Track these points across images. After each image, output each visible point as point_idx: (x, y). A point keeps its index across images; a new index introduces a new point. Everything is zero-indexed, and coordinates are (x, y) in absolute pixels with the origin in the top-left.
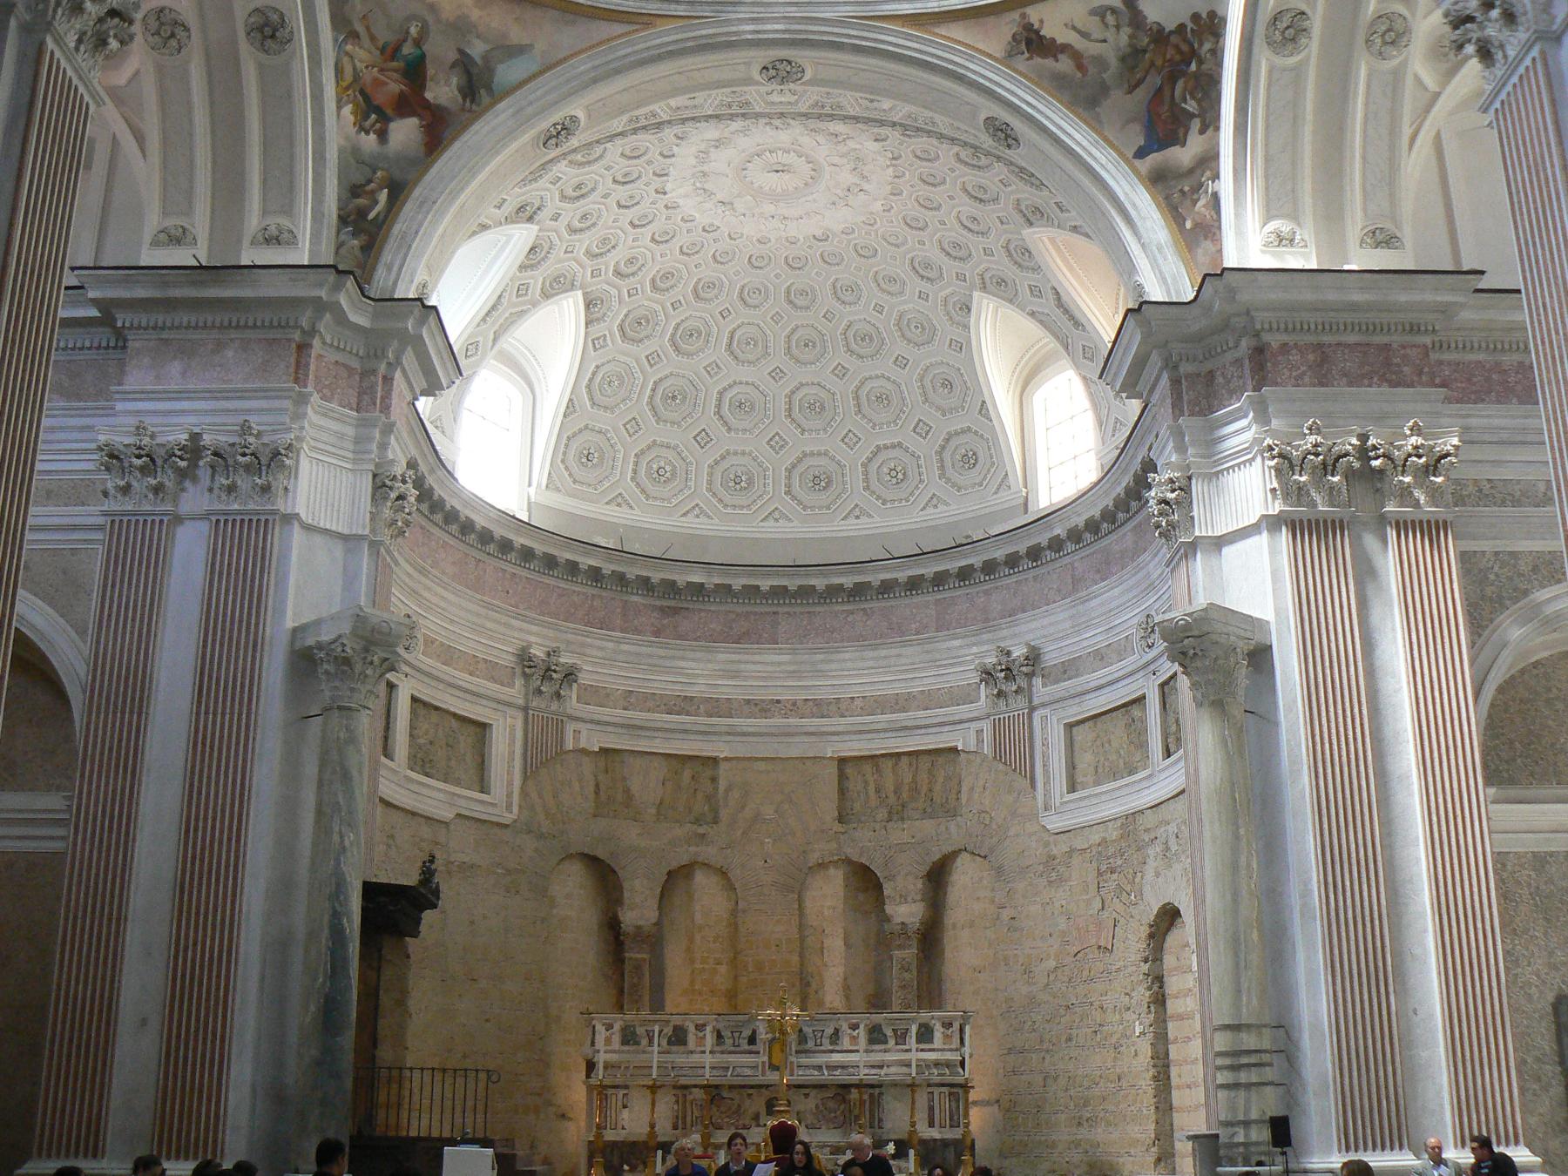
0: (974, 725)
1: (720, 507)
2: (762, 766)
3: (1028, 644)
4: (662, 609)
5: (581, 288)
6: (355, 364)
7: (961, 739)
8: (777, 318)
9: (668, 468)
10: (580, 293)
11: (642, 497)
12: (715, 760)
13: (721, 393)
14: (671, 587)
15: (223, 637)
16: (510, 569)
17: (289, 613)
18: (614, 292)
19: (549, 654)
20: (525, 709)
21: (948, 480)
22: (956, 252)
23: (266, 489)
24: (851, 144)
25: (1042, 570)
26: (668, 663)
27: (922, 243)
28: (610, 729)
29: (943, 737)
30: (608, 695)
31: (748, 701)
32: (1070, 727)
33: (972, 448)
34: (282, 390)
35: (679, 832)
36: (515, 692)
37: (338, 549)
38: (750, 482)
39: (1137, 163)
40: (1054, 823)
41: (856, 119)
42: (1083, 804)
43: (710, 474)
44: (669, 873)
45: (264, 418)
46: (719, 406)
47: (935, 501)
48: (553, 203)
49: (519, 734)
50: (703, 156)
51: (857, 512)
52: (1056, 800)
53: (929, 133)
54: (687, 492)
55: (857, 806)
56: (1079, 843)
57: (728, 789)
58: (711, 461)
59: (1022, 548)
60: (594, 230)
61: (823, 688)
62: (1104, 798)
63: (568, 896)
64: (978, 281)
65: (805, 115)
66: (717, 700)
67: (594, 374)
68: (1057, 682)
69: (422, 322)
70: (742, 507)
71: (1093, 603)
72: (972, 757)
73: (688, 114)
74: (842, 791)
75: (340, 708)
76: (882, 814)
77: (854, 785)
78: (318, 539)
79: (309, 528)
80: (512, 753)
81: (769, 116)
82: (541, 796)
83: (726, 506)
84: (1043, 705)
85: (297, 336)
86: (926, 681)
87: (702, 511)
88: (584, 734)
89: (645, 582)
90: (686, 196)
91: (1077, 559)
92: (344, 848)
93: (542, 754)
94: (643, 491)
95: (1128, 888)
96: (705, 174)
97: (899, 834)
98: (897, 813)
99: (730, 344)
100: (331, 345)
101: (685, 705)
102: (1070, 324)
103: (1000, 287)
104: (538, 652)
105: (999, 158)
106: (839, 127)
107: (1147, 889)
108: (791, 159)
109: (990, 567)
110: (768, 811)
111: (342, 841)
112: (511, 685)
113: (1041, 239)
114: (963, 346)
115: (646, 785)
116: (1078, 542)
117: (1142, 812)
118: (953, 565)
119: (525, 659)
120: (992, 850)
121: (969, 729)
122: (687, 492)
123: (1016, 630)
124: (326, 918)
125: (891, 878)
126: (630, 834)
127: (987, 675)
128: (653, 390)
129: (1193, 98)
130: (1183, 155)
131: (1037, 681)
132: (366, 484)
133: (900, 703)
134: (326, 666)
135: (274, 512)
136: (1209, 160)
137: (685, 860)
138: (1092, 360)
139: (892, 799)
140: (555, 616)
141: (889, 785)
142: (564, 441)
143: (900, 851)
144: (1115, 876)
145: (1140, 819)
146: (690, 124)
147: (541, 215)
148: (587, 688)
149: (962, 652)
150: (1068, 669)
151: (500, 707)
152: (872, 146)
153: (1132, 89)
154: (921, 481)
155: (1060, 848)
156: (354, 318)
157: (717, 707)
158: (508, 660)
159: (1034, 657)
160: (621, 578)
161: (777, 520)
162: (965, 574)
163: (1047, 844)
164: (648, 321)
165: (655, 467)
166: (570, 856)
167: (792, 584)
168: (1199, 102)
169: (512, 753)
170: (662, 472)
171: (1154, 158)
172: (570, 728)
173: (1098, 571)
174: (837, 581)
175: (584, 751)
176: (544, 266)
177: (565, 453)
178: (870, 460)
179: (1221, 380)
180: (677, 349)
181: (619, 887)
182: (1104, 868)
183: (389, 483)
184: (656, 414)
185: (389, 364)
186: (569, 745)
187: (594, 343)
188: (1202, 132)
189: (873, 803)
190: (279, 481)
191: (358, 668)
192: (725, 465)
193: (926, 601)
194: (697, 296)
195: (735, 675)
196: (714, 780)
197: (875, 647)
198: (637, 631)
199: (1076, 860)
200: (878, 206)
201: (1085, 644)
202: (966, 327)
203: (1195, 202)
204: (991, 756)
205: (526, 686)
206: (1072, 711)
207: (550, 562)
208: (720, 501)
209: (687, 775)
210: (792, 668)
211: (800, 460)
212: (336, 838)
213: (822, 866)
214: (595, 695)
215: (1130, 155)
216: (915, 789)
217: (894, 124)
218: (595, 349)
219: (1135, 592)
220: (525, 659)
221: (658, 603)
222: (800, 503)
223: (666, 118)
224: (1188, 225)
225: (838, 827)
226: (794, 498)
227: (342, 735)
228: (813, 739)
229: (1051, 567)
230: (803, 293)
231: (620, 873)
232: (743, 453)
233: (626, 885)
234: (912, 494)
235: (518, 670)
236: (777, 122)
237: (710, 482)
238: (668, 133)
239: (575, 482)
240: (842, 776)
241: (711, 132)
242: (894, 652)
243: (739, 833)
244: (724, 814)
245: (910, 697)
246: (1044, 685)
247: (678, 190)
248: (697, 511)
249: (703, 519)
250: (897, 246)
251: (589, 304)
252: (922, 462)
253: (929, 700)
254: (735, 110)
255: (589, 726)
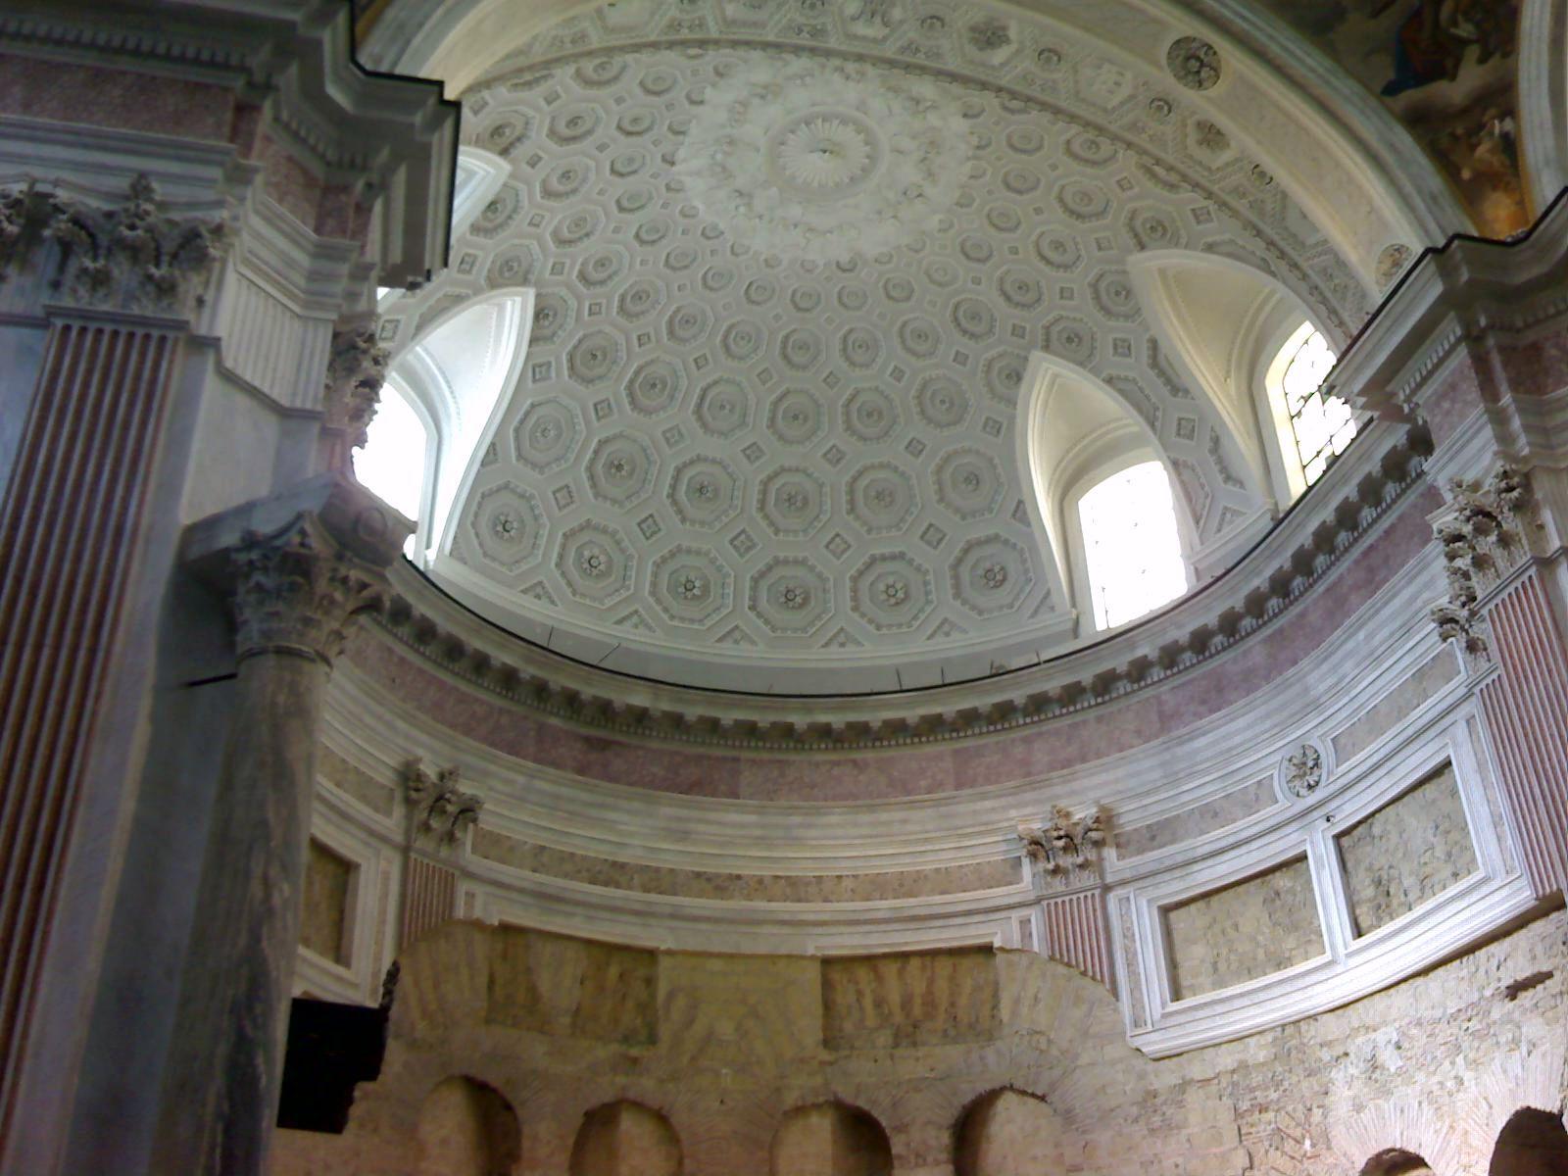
0: (1016, 915)
1: (665, 617)
2: (716, 965)
3: (1097, 802)
4: (587, 740)
5: (537, 285)
6: (318, 170)
7: (1000, 933)
8: (764, 376)
9: (602, 558)
10: (531, 293)
11: (569, 591)
12: (651, 955)
13: (679, 471)
14: (605, 710)
15: (54, 513)
16: (401, 650)
17: (185, 500)
18: (573, 303)
19: (442, 777)
20: (405, 850)
21: (965, 602)
22: (1020, 294)
23: (166, 290)
24: (933, 119)
25: (1113, 707)
26: (594, 812)
27: (977, 281)
28: (514, 895)
29: (973, 931)
30: (512, 849)
31: (698, 875)
32: (1166, 911)
33: (1005, 557)
34: (211, 150)
35: (603, 1052)
36: (392, 823)
37: (270, 424)
38: (706, 589)
39: (1388, 100)
40: (1154, 1043)
41: (954, 77)
42: (1200, 1014)
43: (655, 575)
44: (587, 1114)
45: (180, 188)
46: (674, 487)
47: (946, 628)
48: (538, 140)
49: (394, 888)
50: (739, 111)
51: (842, 638)
52: (1341, 951)
53: (1044, 106)
54: (624, 594)
55: (848, 1027)
56: (1197, 1070)
57: (671, 995)
58: (656, 557)
59: (1086, 676)
60: (573, 199)
61: (800, 861)
62: (1238, 1003)
63: (445, 1142)
64: (1040, 337)
65: (892, 63)
66: (657, 870)
67: (527, 414)
68: (1141, 851)
69: (435, 124)
70: (692, 621)
71: (1201, 742)
72: (1015, 957)
73: (744, 34)
74: (828, 1006)
75: (281, 651)
76: (884, 1038)
77: (844, 997)
78: (242, 401)
79: (229, 377)
80: (383, 912)
81: (845, 56)
82: (416, 983)
83: (672, 617)
84: (1124, 883)
85: (239, 83)
86: (944, 856)
87: (642, 621)
88: (479, 902)
89: (572, 699)
90: (698, 173)
91: (1164, 690)
92: (270, 911)
93: (424, 918)
94: (569, 584)
95: (1298, 1133)
96: (732, 142)
97: (912, 1065)
98: (907, 1035)
99: (700, 405)
100: (287, 126)
101: (613, 873)
102: (1165, 391)
103: (1073, 344)
104: (430, 770)
105: (1129, 145)
106: (926, 88)
107: (1338, 1134)
108: (846, 134)
109: (1039, 704)
110: (726, 1029)
111: (268, 896)
112: (388, 813)
113: (1148, 265)
114: (1004, 430)
115: (560, 983)
116: (1138, 681)
117: (1314, 1017)
118: (984, 701)
119: (409, 777)
120: (1053, 1086)
121: (1014, 921)
122: (624, 594)
123: (1076, 785)
124: (223, 1049)
125: (901, 1128)
126: (536, 1052)
127: (1037, 847)
128: (596, 452)
129: (1468, 20)
130: (1456, 90)
131: (1110, 853)
132: (321, 343)
133: (908, 884)
134: (258, 577)
135: (181, 326)
136: (1501, 97)
137: (607, 1098)
138: (1190, 437)
139: (898, 1018)
140: (453, 726)
141: (894, 997)
142: (478, 498)
143: (915, 1097)
144: (1270, 1115)
145: (1309, 1030)
146: (741, 52)
147: (520, 151)
148: (496, 840)
149: (994, 817)
150: (1156, 835)
151: (372, 841)
152: (958, 124)
153: (1376, 14)
154: (928, 602)
155: (1165, 1078)
156: (334, 92)
157: (657, 880)
158: (386, 777)
159: (1105, 820)
160: (541, 690)
161: (736, 642)
162: (1004, 713)
163: (1142, 1076)
164: (605, 356)
165: (587, 554)
166: (449, 1080)
167: (764, 719)
168: (1477, 24)
169: (383, 912)
170: (594, 562)
171: (1411, 96)
172: (463, 887)
173: (1203, 702)
174: (823, 718)
175: (478, 925)
176: (502, 235)
177: (476, 515)
178: (861, 573)
179: (1554, 352)
180: (633, 402)
181: (513, 1133)
182: (1244, 1106)
183: (363, 345)
184: (594, 486)
185: (369, 186)
186: (460, 912)
187: (533, 371)
188: (1483, 60)
189: (871, 1021)
190: (192, 284)
191: (322, 586)
192: (671, 566)
193: (940, 749)
194: (671, 333)
195: (684, 836)
196: (650, 982)
197: (872, 809)
198: (556, 764)
199: (1193, 1097)
200: (934, 222)
201: (1186, 798)
202: (1012, 402)
203: (1473, 148)
204: (1045, 954)
205: (409, 817)
206: (1165, 889)
207: (454, 650)
208: (666, 610)
209: (613, 971)
210: (758, 832)
211: (770, 568)
212: (256, 889)
213: (800, 1110)
214: (496, 846)
215: (1378, 90)
216: (930, 1002)
217: (999, 90)
218: (535, 380)
219: (1276, 719)
220: (409, 777)
221: (585, 731)
222: (767, 622)
223: (714, 34)
224: (1466, 174)
225: (825, 1055)
226: (759, 615)
227: (281, 699)
228: (786, 930)
229: (1123, 703)
230: (803, 346)
231: (521, 1113)
232: (698, 553)
233: (526, 1130)
234: (915, 618)
235: (399, 795)
236: (851, 67)
237: (654, 585)
238: (712, 57)
239: (485, 555)
240: (827, 985)
241: (760, 70)
242: (898, 815)
243: (685, 1060)
244: (665, 1032)
245: (920, 878)
246: (1120, 857)
247: (692, 161)
248: (635, 619)
249: (641, 630)
250: (940, 285)
251: (540, 315)
252: (930, 577)
253: (946, 880)
254: (805, 40)
255: (489, 889)
